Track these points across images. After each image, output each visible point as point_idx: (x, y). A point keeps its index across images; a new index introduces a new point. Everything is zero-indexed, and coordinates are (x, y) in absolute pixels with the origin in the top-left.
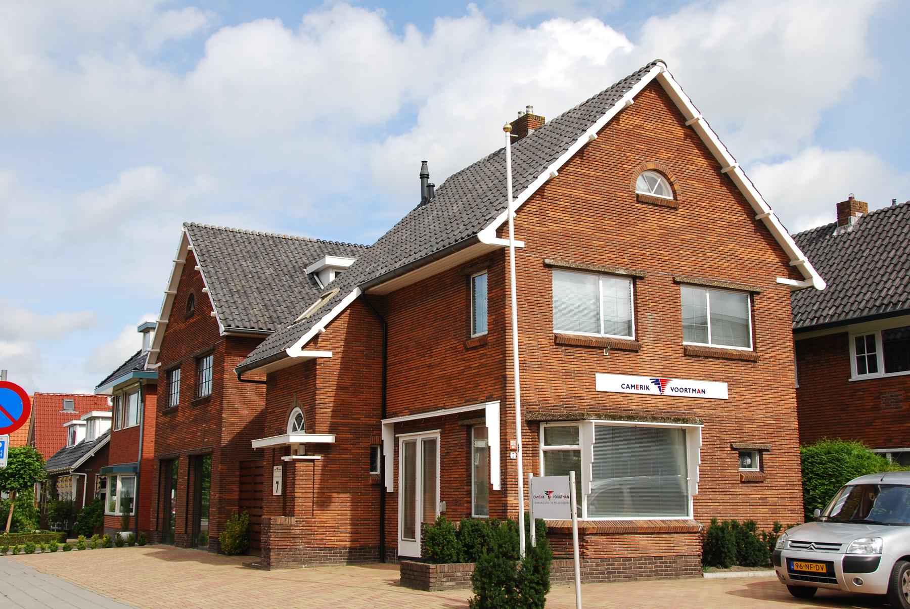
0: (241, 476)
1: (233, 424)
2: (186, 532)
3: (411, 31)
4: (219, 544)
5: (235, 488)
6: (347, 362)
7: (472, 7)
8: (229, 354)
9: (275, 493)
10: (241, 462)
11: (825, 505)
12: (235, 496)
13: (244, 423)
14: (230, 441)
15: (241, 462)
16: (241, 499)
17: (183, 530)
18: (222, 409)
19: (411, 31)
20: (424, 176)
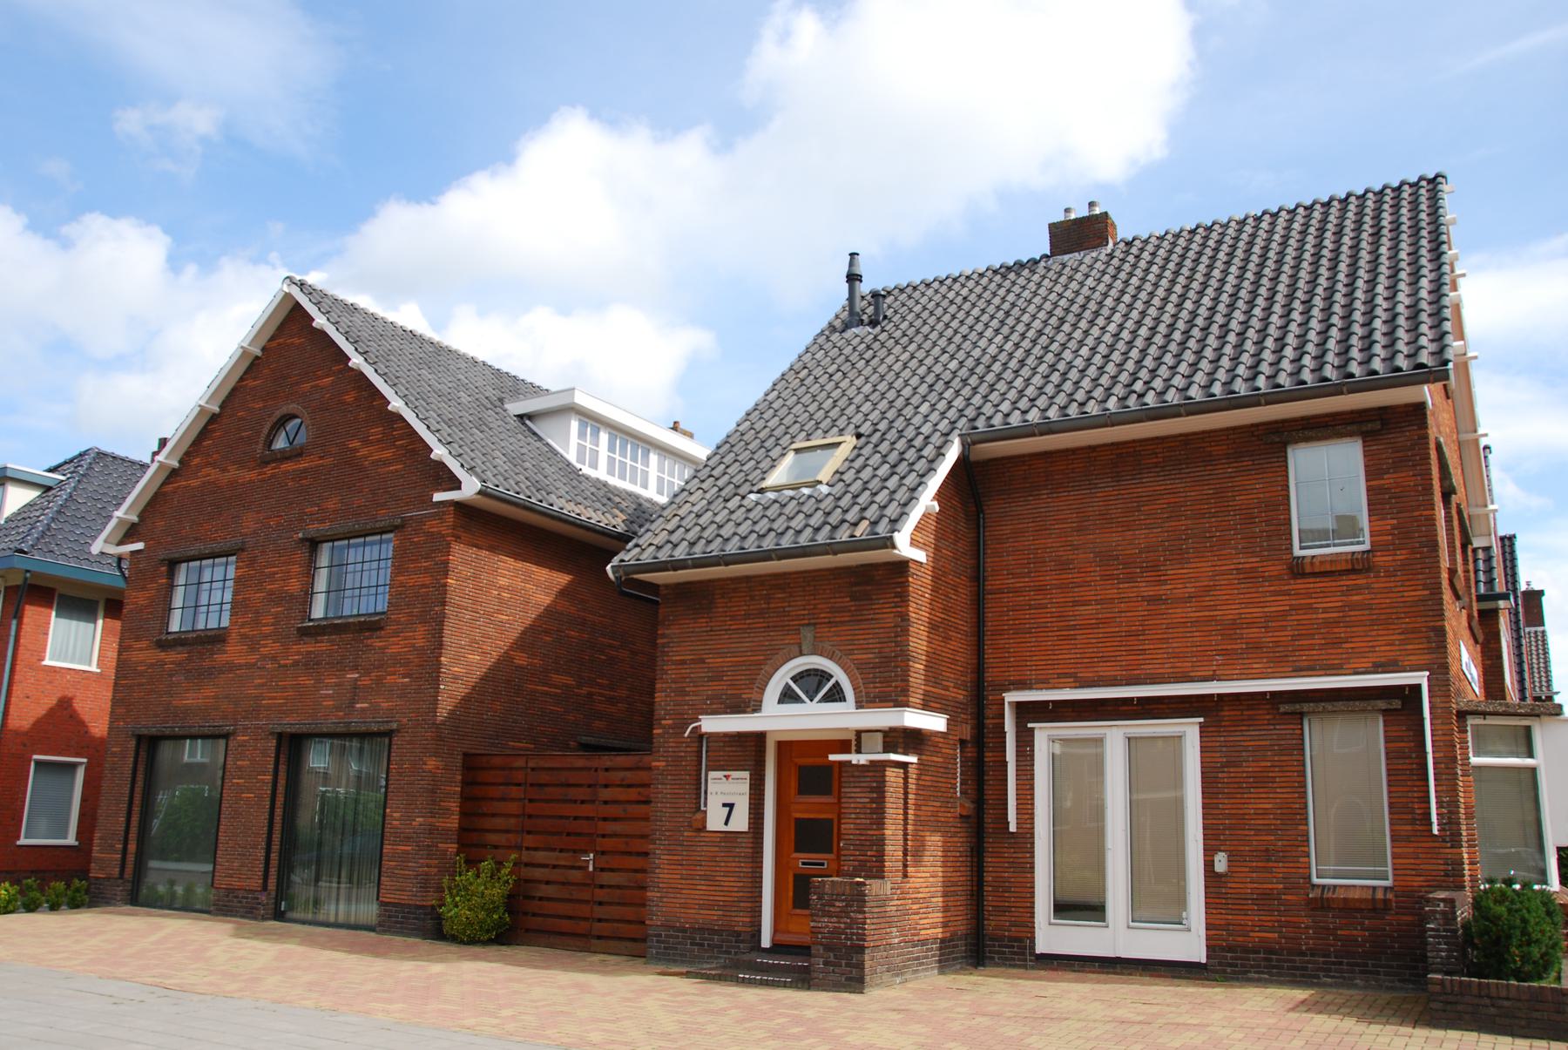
0: (465, 783)
1: (456, 678)
2: (265, 887)
3: (191, 270)
4: (439, 919)
5: (454, 805)
6: (937, 555)
7: (274, 256)
8: (457, 538)
9: (715, 822)
10: (465, 754)
11: (1499, 918)
12: (453, 822)
13: (473, 680)
14: (451, 713)
15: (465, 754)
16: (463, 829)
17: (256, 883)
18: (441, 645)
19: (191, 270)
20: (853, 278)
